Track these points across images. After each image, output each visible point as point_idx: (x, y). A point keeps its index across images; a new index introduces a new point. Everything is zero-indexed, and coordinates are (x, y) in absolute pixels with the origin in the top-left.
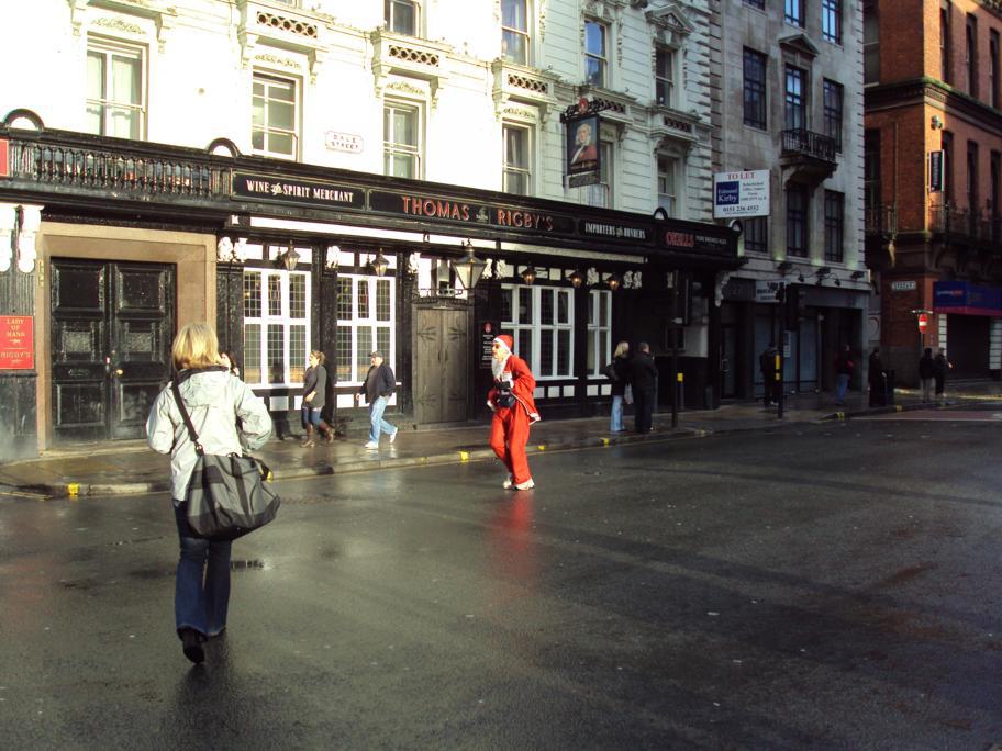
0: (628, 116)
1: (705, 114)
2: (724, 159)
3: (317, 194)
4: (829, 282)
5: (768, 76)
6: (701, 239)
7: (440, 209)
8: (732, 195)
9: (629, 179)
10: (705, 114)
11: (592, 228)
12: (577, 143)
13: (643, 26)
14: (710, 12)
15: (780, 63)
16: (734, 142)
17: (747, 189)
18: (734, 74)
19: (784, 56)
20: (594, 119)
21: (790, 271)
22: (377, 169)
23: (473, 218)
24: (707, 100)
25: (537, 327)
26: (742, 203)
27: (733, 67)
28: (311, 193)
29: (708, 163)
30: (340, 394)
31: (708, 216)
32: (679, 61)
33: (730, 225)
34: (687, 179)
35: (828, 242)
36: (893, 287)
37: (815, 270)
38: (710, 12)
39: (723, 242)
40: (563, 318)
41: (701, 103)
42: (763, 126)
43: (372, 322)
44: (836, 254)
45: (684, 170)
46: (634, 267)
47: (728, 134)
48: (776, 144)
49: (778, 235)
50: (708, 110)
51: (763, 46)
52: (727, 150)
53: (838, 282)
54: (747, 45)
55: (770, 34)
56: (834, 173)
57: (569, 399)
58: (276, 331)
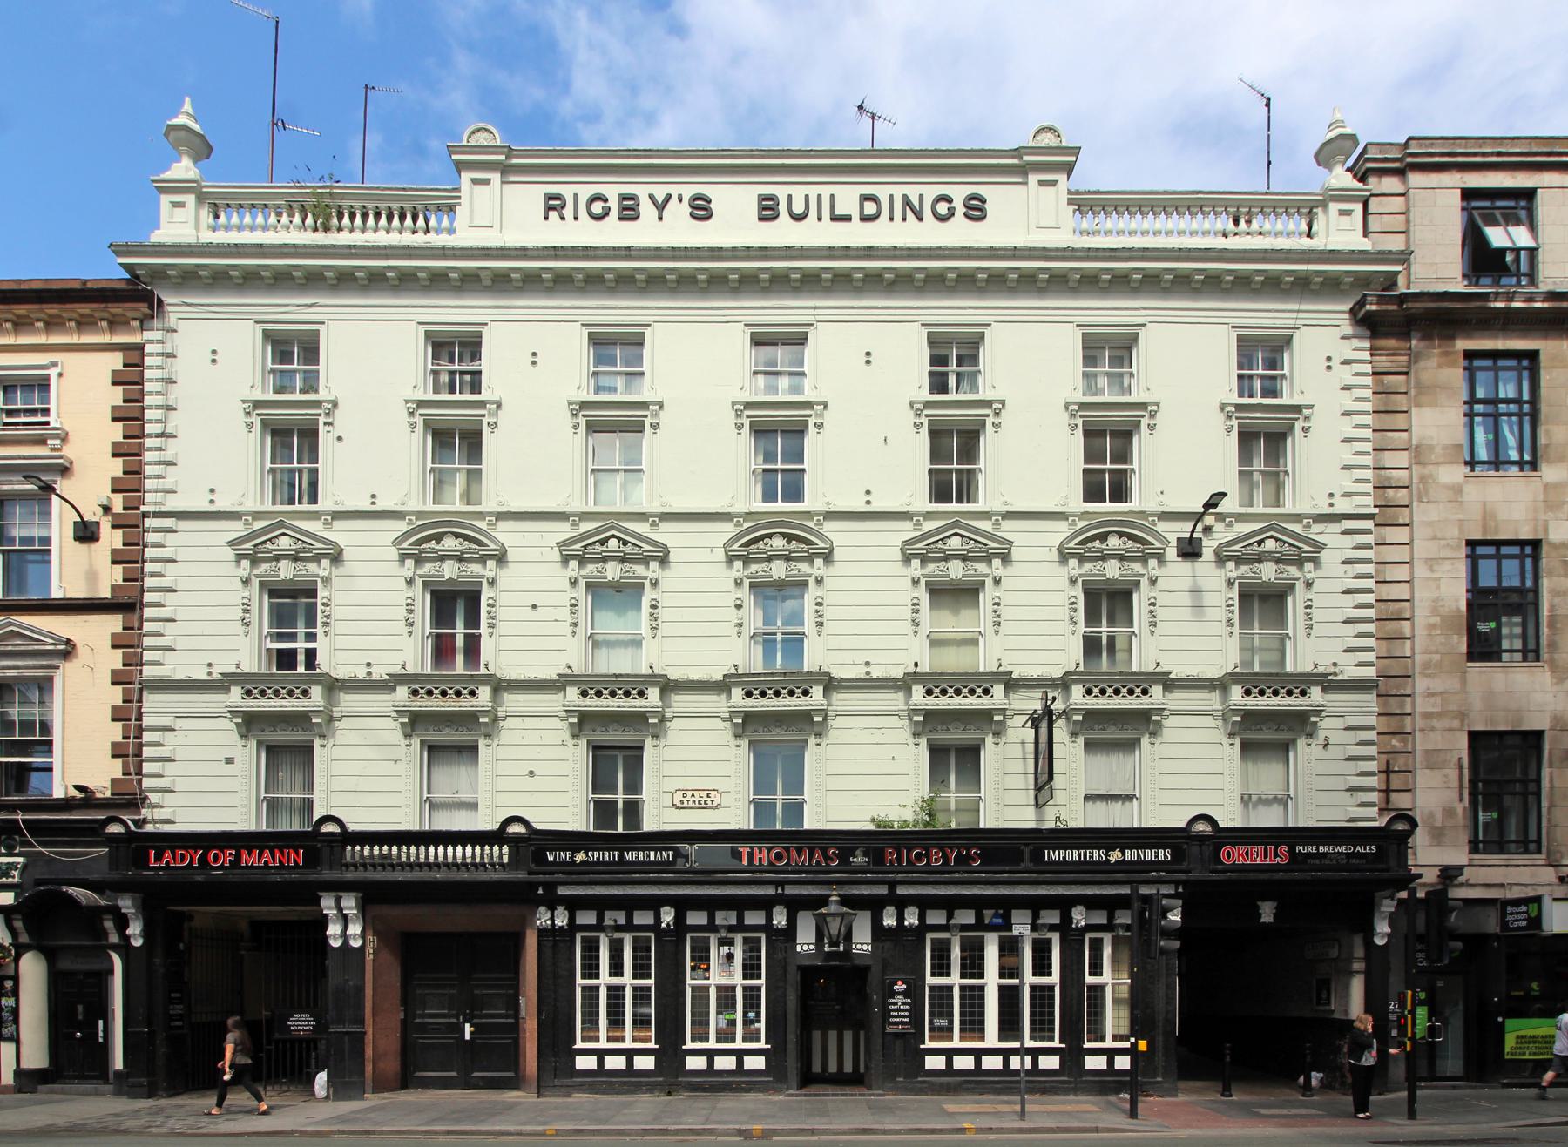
3: (628, 856)
7: (795, 856)
9: (1216, 782)
11: (1054, 855)
14: (1376, 510)
22: (1334, 818)
28: (621, 856)
38: (1376, 510)
57: (1122, 1072)
58: (616, 993)
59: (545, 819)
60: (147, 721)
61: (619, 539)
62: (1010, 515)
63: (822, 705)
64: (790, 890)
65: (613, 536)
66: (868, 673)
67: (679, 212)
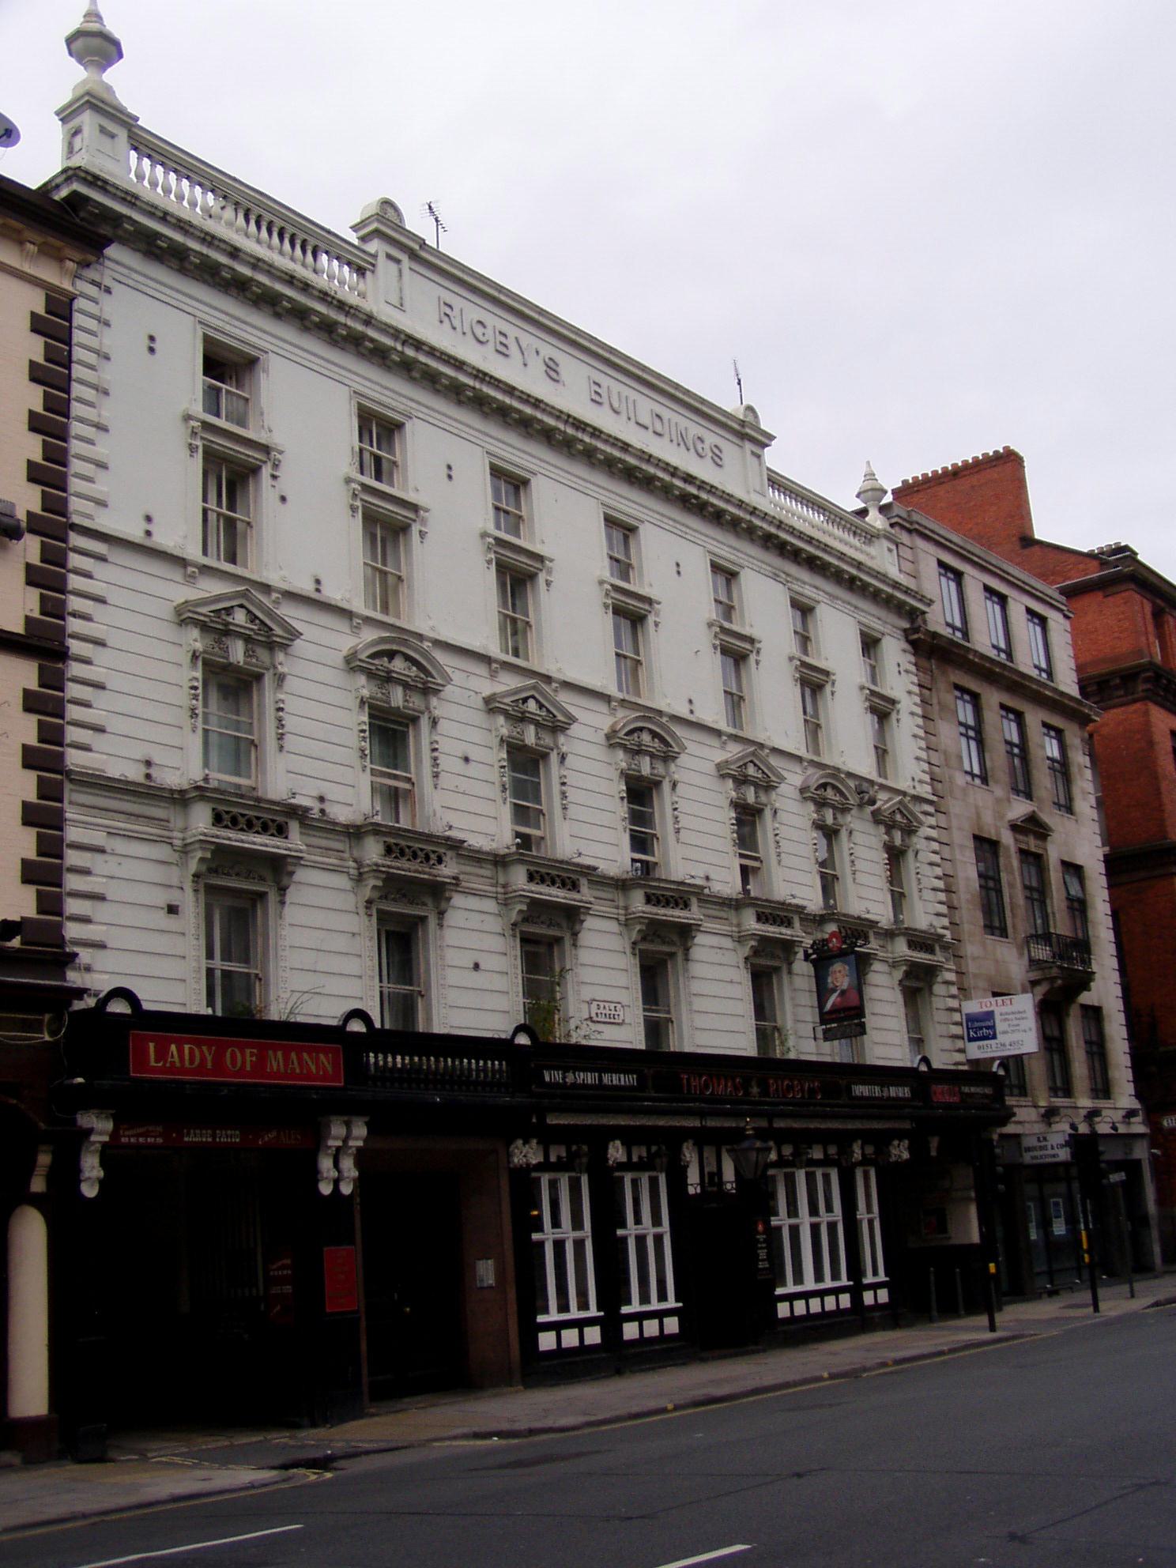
0: (694, 914)
1: (944, 928)
2: (969, 982)
3: (606, 1079)
4: (1103, 1128)
5: (1002, 868)
6: (966, 1090)
8: (988, 1028)
10: (944, 928)
12: (831, 986)
13: (869, 827)
14: (935, 798)
15: (1013, 850)
16: (978, 958)
17: (1006, 1020)
18: (968, 872)
19: (1016, 840)
20: (852, 957)
21: (1057, 1119)
23: (747, 1093)
24: (943, 909)
25: (805, 1220)
26: (1000, 1038)
27: (965, 863)
29: (954, 990)
30: (865, 1290)
31: (960, 1057)
32: (910, 864)
33: (994, 1069)
34: (935, 1011)
35: (1092, 1077)
36: (1165, 1123)
37: (1083, 1112)
38: (935, 798)
39: (988, 1091)
40: (829, 1208)
41: (938, 915)
42: (1003, 933)
43: (647, 1227)
44: (1103, 1088)
45: (931, 1002)
46: (900, 1135)
47: (970, 949)
48: (1021, 955)
49: (1037, 1074)
50: (945, 922)
51: (993, 831)
52: (970, 970)
53: (1114, 1128)
54: (977, 833)
55: (999, 816)
56: (1092, 984)
57: (672, 1336)
59: (156, 997)
60: (72, 834)
61: (537, 701)
62: (567, 685)
63: (301, 851)
64: (779, 1124)
65: (533, 697)
66: (148, 776)
67: (537, 367)
